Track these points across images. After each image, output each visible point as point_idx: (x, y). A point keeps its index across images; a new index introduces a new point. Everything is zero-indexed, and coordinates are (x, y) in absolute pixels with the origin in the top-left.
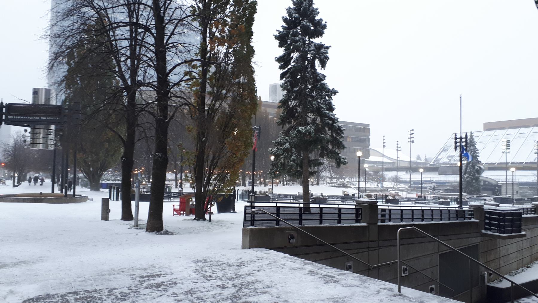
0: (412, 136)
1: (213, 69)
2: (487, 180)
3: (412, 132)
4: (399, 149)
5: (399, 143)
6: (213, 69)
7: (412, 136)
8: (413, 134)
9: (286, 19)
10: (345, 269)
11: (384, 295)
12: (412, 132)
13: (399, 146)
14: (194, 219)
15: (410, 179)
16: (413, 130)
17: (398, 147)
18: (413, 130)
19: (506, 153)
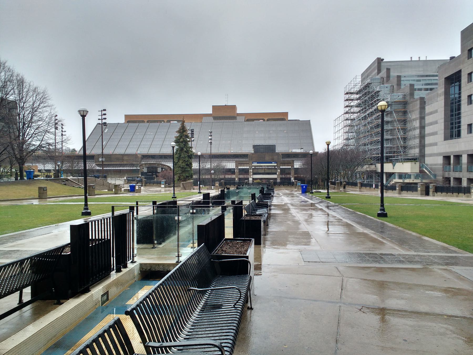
0: (104, 117)
1: (33, 261)
2: (419, 75)
3: (104, 112)
4: (64, 133)
5: (63, 127)
6: (33, 261)
7: (104, 117)
8: (105, 114)
9: (256, 244)
10: (105, 171)
11: (182, 163)
12: (104, 112)
13: (63, 130)
14: (258, 243)
15: (102, 152)
16: (105, 110)
17: (62, 131)
18: (105, 110)
19: (191, 141)
